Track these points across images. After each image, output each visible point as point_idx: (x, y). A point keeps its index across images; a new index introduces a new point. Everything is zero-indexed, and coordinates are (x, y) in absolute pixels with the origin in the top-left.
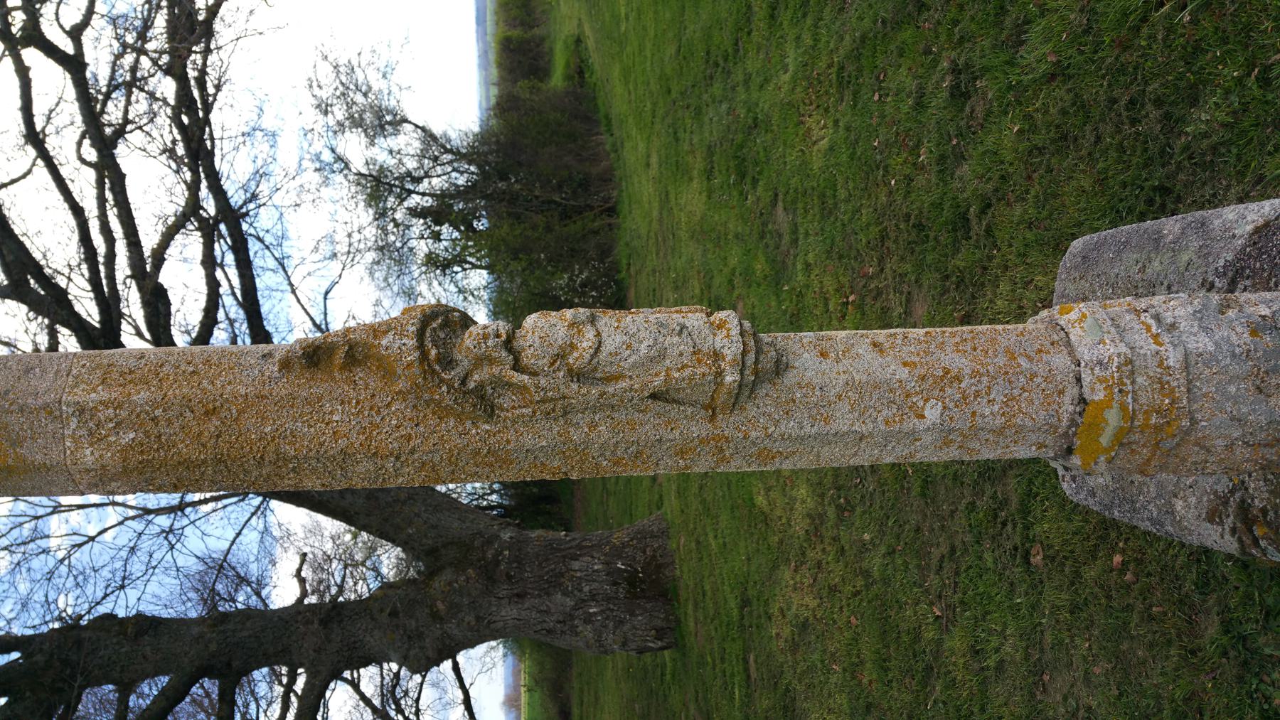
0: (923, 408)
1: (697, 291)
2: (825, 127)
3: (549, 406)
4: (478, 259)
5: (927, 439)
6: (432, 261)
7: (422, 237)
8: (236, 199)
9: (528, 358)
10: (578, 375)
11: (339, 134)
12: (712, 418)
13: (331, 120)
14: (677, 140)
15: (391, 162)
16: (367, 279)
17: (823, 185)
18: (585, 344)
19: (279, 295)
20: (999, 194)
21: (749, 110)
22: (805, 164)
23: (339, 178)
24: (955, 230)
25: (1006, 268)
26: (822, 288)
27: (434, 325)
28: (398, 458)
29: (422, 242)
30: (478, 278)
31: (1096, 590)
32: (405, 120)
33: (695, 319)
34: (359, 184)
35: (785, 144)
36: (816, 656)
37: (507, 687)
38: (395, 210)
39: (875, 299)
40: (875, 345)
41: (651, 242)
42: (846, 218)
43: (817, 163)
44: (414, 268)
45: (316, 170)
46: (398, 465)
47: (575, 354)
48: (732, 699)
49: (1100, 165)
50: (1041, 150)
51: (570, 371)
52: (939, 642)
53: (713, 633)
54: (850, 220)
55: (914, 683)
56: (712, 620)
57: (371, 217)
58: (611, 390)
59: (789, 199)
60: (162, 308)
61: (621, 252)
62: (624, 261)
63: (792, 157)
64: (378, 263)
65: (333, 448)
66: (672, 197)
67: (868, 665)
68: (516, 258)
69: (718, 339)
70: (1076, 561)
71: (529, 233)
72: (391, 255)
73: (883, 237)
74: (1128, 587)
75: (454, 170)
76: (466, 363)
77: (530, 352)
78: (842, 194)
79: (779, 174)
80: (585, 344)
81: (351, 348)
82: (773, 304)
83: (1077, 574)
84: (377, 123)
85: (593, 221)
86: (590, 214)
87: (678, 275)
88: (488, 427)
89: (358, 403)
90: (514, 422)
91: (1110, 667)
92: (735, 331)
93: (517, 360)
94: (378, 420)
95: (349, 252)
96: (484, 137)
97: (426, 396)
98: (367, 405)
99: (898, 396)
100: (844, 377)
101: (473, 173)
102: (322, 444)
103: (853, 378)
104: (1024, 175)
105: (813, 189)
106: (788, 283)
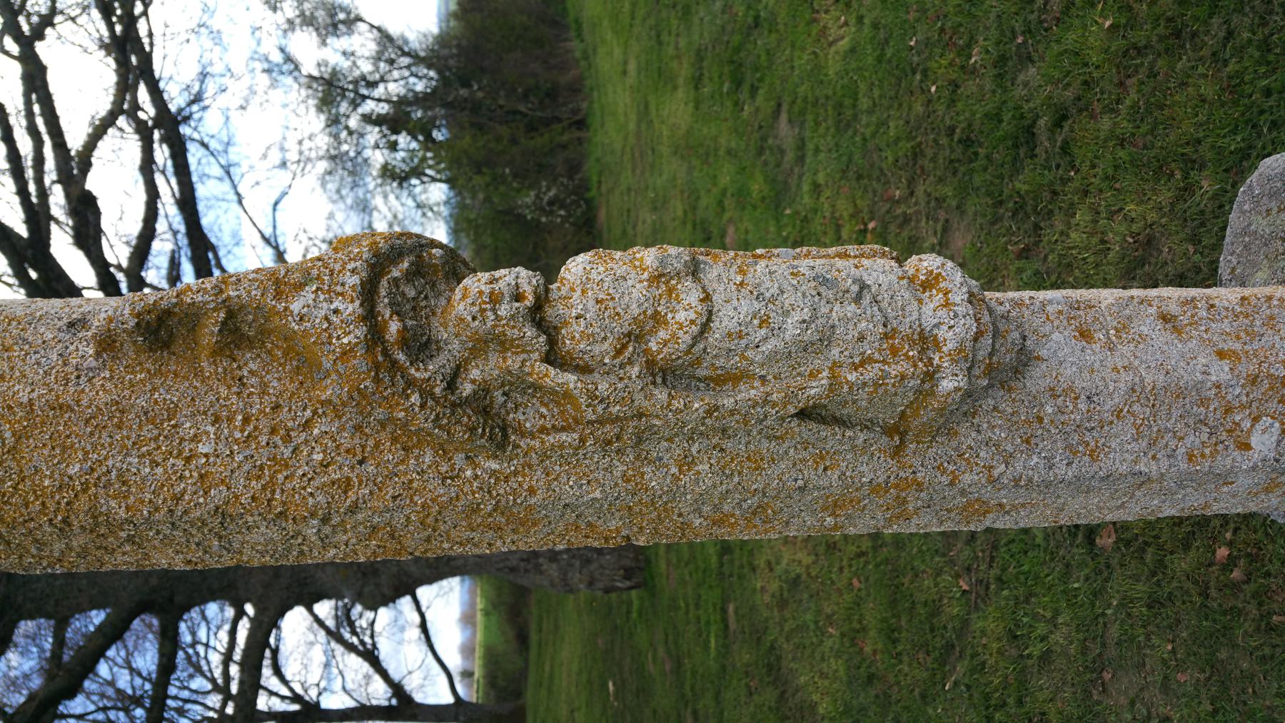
0: (1249, 432)
1: (680, 213)
2: (846, 24)
3: (610, 430)
4: (438, 172)
5: (1243, 482)
6: (388, 173)
7: (377, 146)
8: (176, 100)
9: (573, 339)
10: (663, 371)
11: (289, 33)
12: (897, 452)
13: (280, 18)
14: (660, 43)
15: (345, 64)
16: (319, 190)
17: (840, 93)
18: (681, 316)
19: (224, 205)
20: (1081, 104)
21: (749, 8)
22: (818, 67)
23: (288, 80)
24: (1016, 146)
25: (1086, 193)
26: (833, 213)
27: (396, 273)
28: (325, 520)
29: (377, 152)
30: (438, 192)
31: (1189, 585)
32: (359, 19)
33: (879, 269)
34: (310, 87)
35: (793, 46)
36: (809, 617)
37: (462, 604)
38: (348, 117)
39: (901, 226)
40: (1165, 318)
41: (626, 158)
42: (868, 132)
43: (833, 67)
44: (369, 179)
45: (264, 71)
46: (327, 530)
47: (662, 334)
48: (706, 647)
49: (1231, 68)
50: (1140, 51)
51: (650, 364)
52: (965, 623)
53: (687, 578)
54: (874, 135)
55: (929, 660)
56: (687, 564)
57: (323, 125)
58: (728, 402)
59: (796, 109)
60: (91, 218)
61: (591, 169)
62: (595, 178)
63: (803, 61)
64: (330, 173)
65: (201, 505)
66: (652, 108)
67: (872, 633)
68: (479, 172)
69: (928, 309)
70: (1161, 548)
71: (492, 145)
72: (345, 165)
73: (917, 153)
74: (1235, 586)
75: (412, 75)
76: (456, 345)
77: (578, 328)
78: (864, 103)
79: (784, 80)
80: (681, 316)
81: (231, 314)
82: (772, 229)
83: (1161, 563)
84: (329, 21)
85: (562, 134)
86: (557, 127)
87: (657, 195)
88: (494, 465)
89: (246, 420)
90: (544, 456)
91: (1202, 677)
92: (958, 297)
93: (552, 342)
94: (287, 453)
95: (299, 161)
96: (442, 40)
97: (380, 413)
98: (264, 424)
99: (1213, 412)
100: (1126, 377)
101: (432, 78)
102: (178, 498)
103: (1142, 381)
104: (1116, 80)
105: (827, 98)
106: (790, 206)
